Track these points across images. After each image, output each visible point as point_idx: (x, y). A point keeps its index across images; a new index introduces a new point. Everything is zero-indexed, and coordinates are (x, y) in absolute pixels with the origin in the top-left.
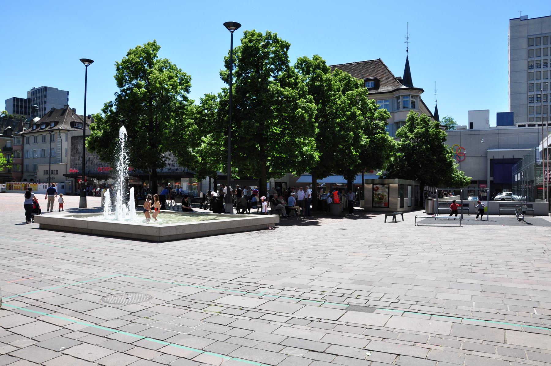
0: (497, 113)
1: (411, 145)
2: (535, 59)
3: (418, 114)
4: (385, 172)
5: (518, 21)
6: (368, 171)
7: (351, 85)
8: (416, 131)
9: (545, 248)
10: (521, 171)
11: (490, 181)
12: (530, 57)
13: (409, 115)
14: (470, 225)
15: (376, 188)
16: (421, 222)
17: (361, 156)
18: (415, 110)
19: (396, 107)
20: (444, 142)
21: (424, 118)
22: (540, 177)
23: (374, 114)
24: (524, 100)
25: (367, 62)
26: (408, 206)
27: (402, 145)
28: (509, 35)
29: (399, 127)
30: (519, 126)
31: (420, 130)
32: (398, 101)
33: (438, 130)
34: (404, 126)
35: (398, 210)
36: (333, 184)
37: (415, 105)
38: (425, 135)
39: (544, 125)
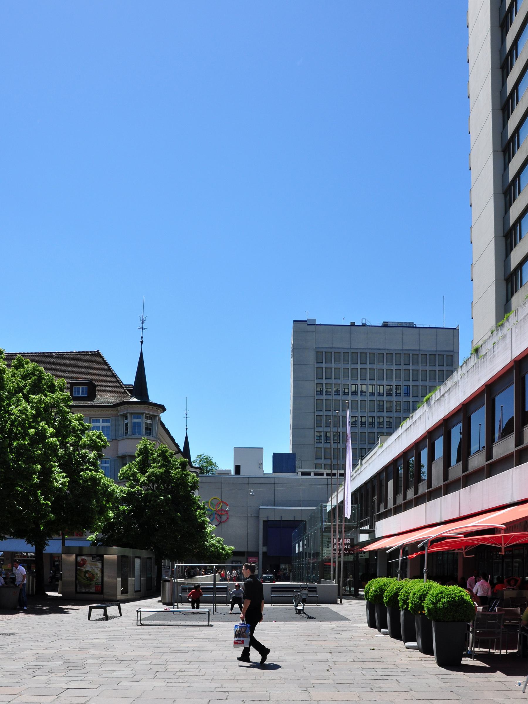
0: (274, 454)
1: (142, 494)
2: (324, 381)
3: (154, 444)
4: (101, 536)
5: (303, 325)
6: (71, 534)
7: (43, 386)
8: (151, 471)
9: (329, 660)
10: (303, 538)
11: (263, 553)
12: (318, 378)
13: (140, 445)
14: (226, 623)
15: (82, 562)
16: (146, 619)
17: (56, 507)
18: (151, 438)
19: (121, 431)
20: (194, 492)
21: (164, 452)
22: (327, 547)
23: (80, 438)
24: (310, 438)
25: (78, 353)
26: (136, 592)
27: (129, 494)
28: (293, 343)
29: (125, 464)
30: (303, 474)
31: (157, 471)
32: (125, 422)
33: (185, 472)
34: (132, 463)
35: (118, 597)
36: (17, 553)
37: (151, 431)
38: (165, 478)
39: (334, 475)
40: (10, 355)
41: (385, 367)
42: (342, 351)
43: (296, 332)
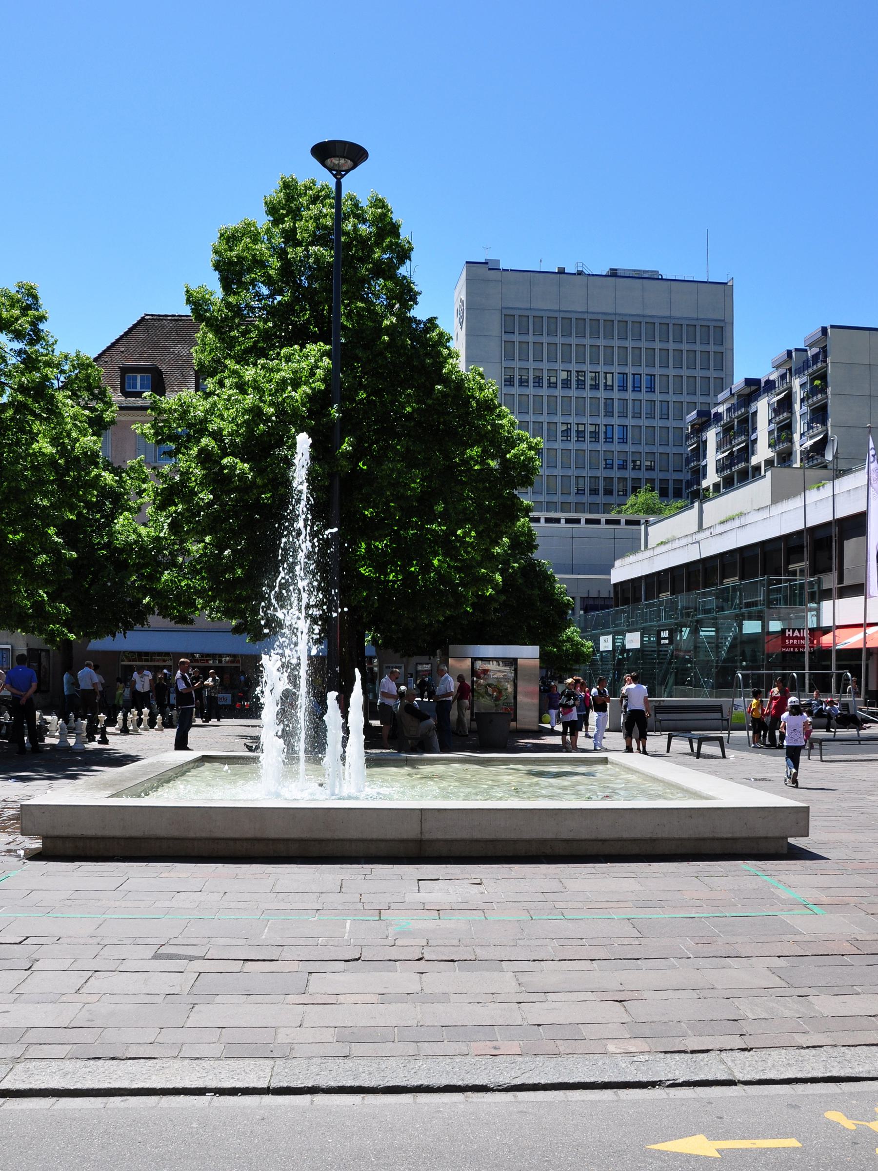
2: (516, 364)
28: (464, 299)
40: (155, 317)
41: (587, 341)
42: (545, 314)
43: (471, 281)
